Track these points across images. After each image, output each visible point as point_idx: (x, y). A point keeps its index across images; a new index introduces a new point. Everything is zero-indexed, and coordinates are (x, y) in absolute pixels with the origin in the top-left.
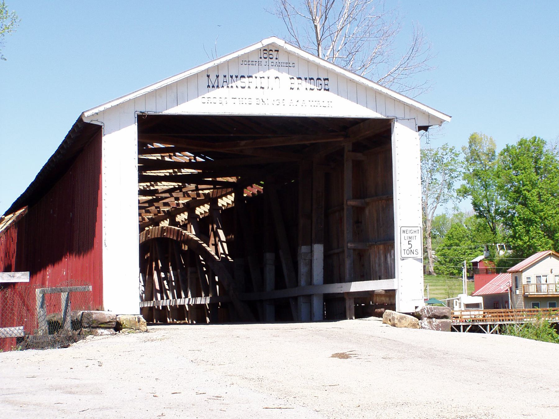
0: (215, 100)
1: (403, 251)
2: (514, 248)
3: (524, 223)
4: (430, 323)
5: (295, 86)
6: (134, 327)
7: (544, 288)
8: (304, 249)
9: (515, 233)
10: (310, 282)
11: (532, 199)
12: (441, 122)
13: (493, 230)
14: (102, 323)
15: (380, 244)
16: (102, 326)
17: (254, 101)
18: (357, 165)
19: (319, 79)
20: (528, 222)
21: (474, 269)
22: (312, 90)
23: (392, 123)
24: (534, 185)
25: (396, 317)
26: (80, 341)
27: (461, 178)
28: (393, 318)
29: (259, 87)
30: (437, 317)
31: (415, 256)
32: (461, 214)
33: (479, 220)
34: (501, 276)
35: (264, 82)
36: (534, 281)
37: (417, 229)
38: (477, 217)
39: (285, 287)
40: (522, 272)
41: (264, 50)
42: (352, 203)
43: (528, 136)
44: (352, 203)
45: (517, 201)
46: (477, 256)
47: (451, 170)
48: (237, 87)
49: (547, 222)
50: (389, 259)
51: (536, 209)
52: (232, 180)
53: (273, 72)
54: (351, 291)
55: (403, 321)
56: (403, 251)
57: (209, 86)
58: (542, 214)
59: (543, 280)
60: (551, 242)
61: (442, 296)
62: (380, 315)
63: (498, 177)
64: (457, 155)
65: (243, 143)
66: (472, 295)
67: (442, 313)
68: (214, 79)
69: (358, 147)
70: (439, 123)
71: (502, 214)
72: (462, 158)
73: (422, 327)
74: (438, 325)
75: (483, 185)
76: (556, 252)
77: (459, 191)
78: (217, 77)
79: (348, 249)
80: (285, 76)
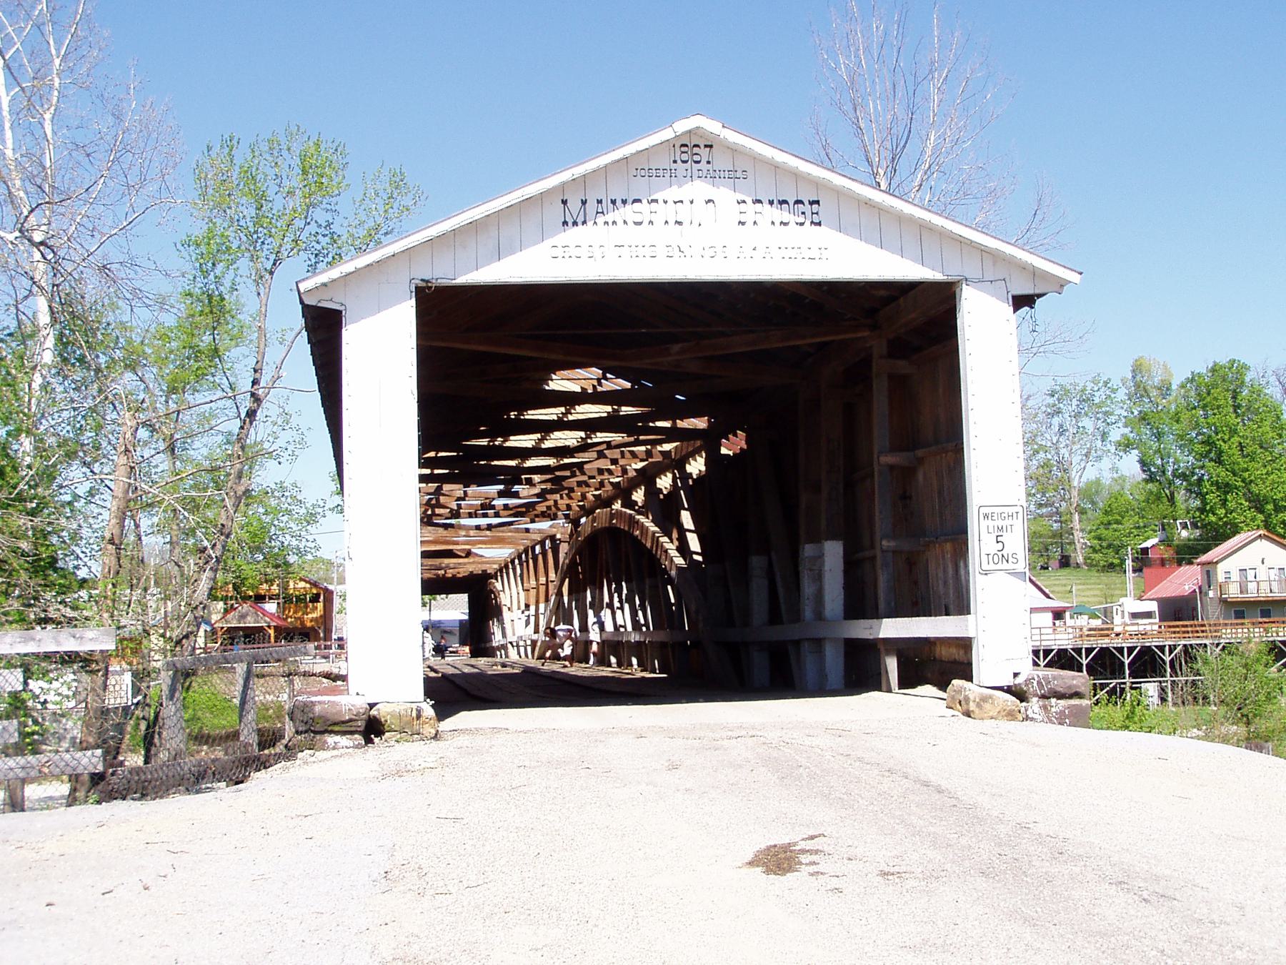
0: (577, 252)
1: (984, 558)
2: (1204, 526)
3: (1218, 488)
4: (1045, 707)
5: (749, 218)
6: (410, 728)
7: (1252, 587)
8: (808, 550)
9: (1204, 502)
10: (819, 615)
11: (1231, 452)
12: (1062, 286)
13: (1171, 499)
14: (335, 724)
15: (946, 541)
16: (336, 728)
17: (661, 251)
18: (899, 384)
19: (798, 202)
20: (1225, 488)
21: (1143, 560)
22: (786, 224)
23: (958, 291)
24: (1233, 432)
25: (971, 697)
26: (279, 765)
27: (1120, 425)
28: (967, 699)
29: (672, 222)
30: (1060, 696)
31: (1010, 566)
32: (1123, 478)
33: (1150, 486)
34: (1185, 569)
35: (683, 212)
36: (1235, 576)
37: (1011, 510)
38: (1147, 481)
39: (782, 623)
40: (1217, 563)
41: (683, 145)
42: (888, 459)
43: (1223, 360)
44: (888, 459)
45: (1206, 457)
46: (1148, 538)
47: (1106, 413)
48: (625, 222)
49: (1254, 489)
50: (962, 572)
51: (1236, 467)
52: (701, 423)
53: (699, 189)
54: (881, 636)
55: (987, 706)
56: (984, 558)
57: (565, 223)
58: (1246, 475)
59: (1250, 575)
60: (1261, 517)
61: (1097, 599)
62: (943, 686)
63: (1177, 421)
64: (1114, 391)
65: (676, 348)
66: (1140, 599)
67: (1070, 687)
68: (575, 206)
69: (899, 348)
70: (1057, 288)
71: (1184, 477)
72: (1121, 395)
73: (1027, 718)
74: (1062, 712)
75: (1153, 434)
76: (1269, 531)
77: (1119, 444)
78: (584, 203)
79: (883, 551)
80: (725, 195)
